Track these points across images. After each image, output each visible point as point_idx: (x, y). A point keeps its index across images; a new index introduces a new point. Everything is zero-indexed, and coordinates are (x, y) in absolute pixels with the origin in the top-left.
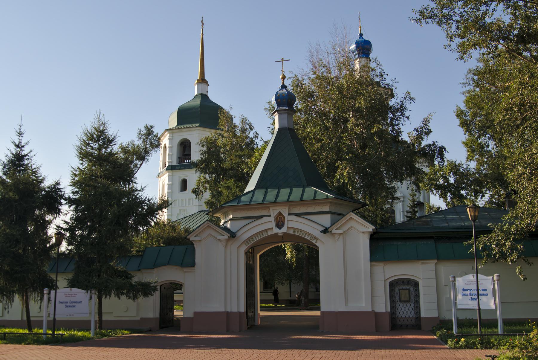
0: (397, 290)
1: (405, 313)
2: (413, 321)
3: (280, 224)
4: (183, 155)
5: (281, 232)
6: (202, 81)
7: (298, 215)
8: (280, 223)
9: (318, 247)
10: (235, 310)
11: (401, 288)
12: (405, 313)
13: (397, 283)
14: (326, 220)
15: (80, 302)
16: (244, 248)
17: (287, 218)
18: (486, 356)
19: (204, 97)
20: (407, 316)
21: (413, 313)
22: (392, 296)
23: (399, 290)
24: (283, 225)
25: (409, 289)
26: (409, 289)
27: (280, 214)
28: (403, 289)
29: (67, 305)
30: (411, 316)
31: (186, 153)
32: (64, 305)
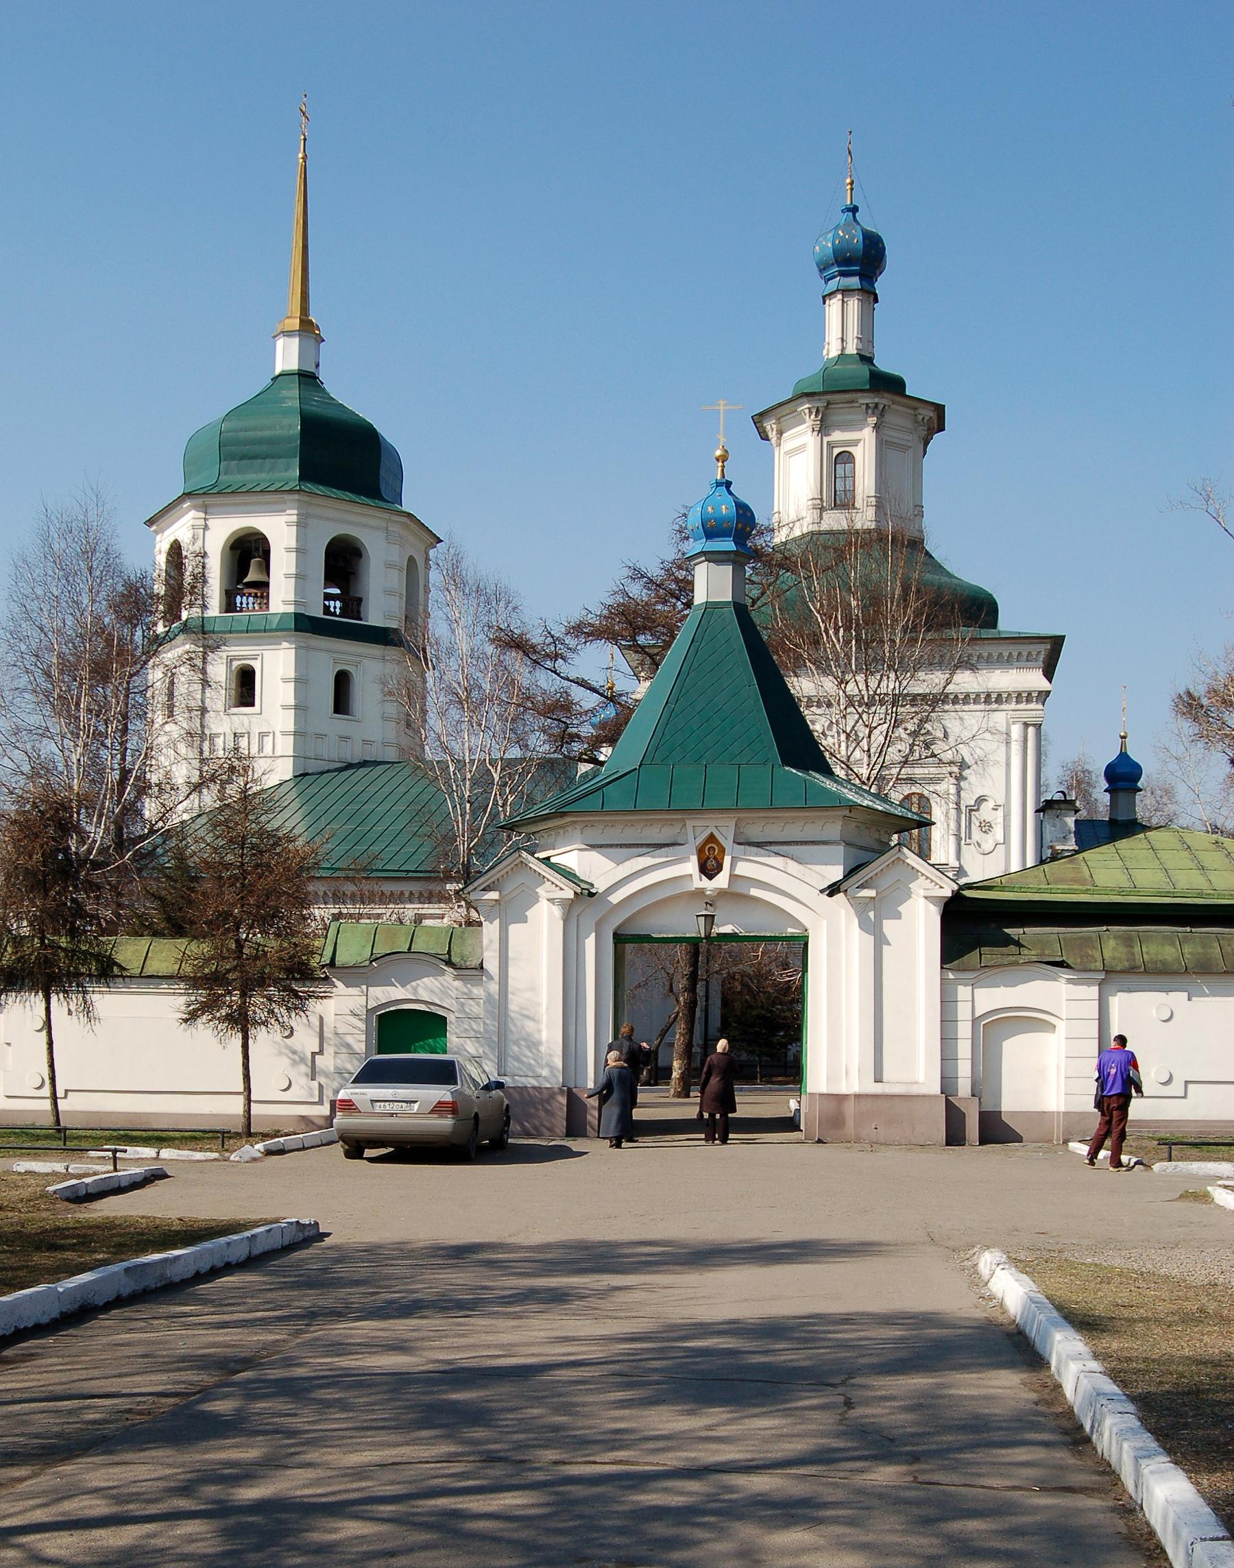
6: (307, 328)
8: (711, 863)
19: (307, 378)
24: (719, 868)
27: (712, 838)
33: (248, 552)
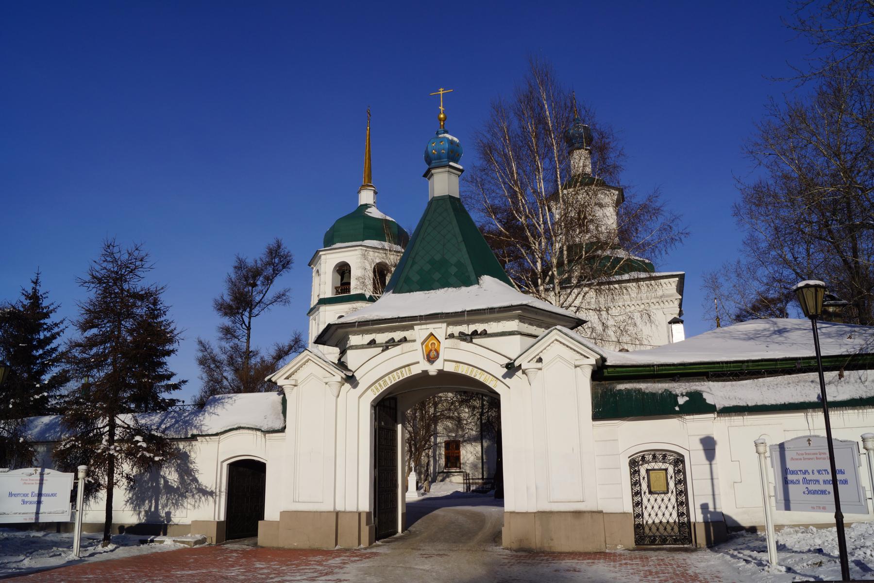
0: (643, 472)
1: (653, 515)
2: (676, 529)
3: (431, 358)
4: (342, 284)
5: (432, 370)
7: (463, 337)
8: (433, 354)
9: (499, 395)
10: (351, 507)
11: (649, 468)
12: (653, 515)
13: (643, 457)
14: (512, 347)
15: (54, 495)
16: (372, 395)
17: (445, 344)
18: (627, 351)
20: (664, 521)
21: (675, 515)
22: (635, 484)
23: (648, 471)
24: (437, 357)
25: (666, 470)
26: (666, 470)
28: (654, 470)
29: (26, 499)
30: (671, 521)
31: (345, 281)
32: (19, 499)
33: (343, 270)
